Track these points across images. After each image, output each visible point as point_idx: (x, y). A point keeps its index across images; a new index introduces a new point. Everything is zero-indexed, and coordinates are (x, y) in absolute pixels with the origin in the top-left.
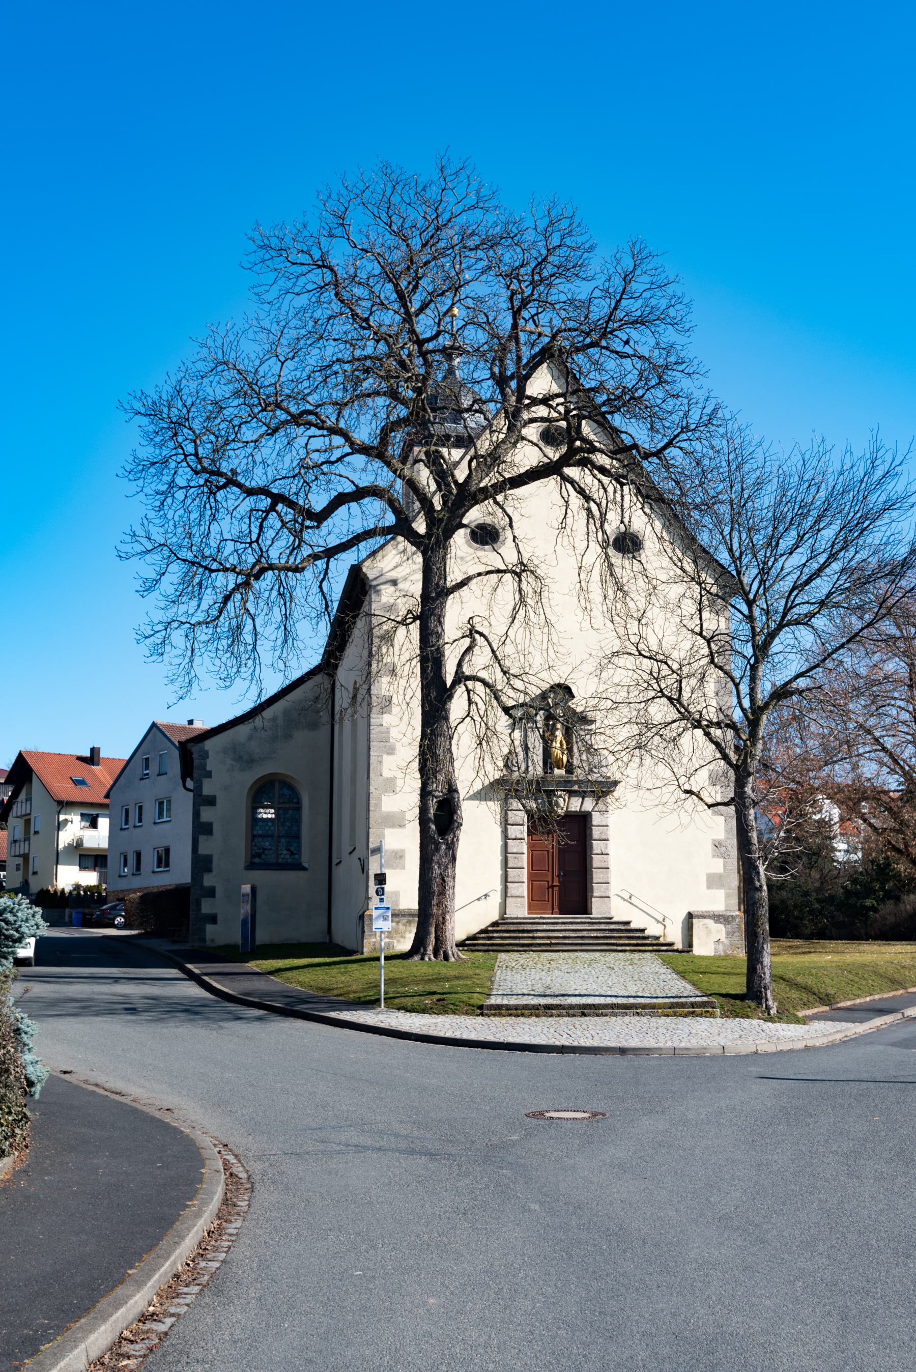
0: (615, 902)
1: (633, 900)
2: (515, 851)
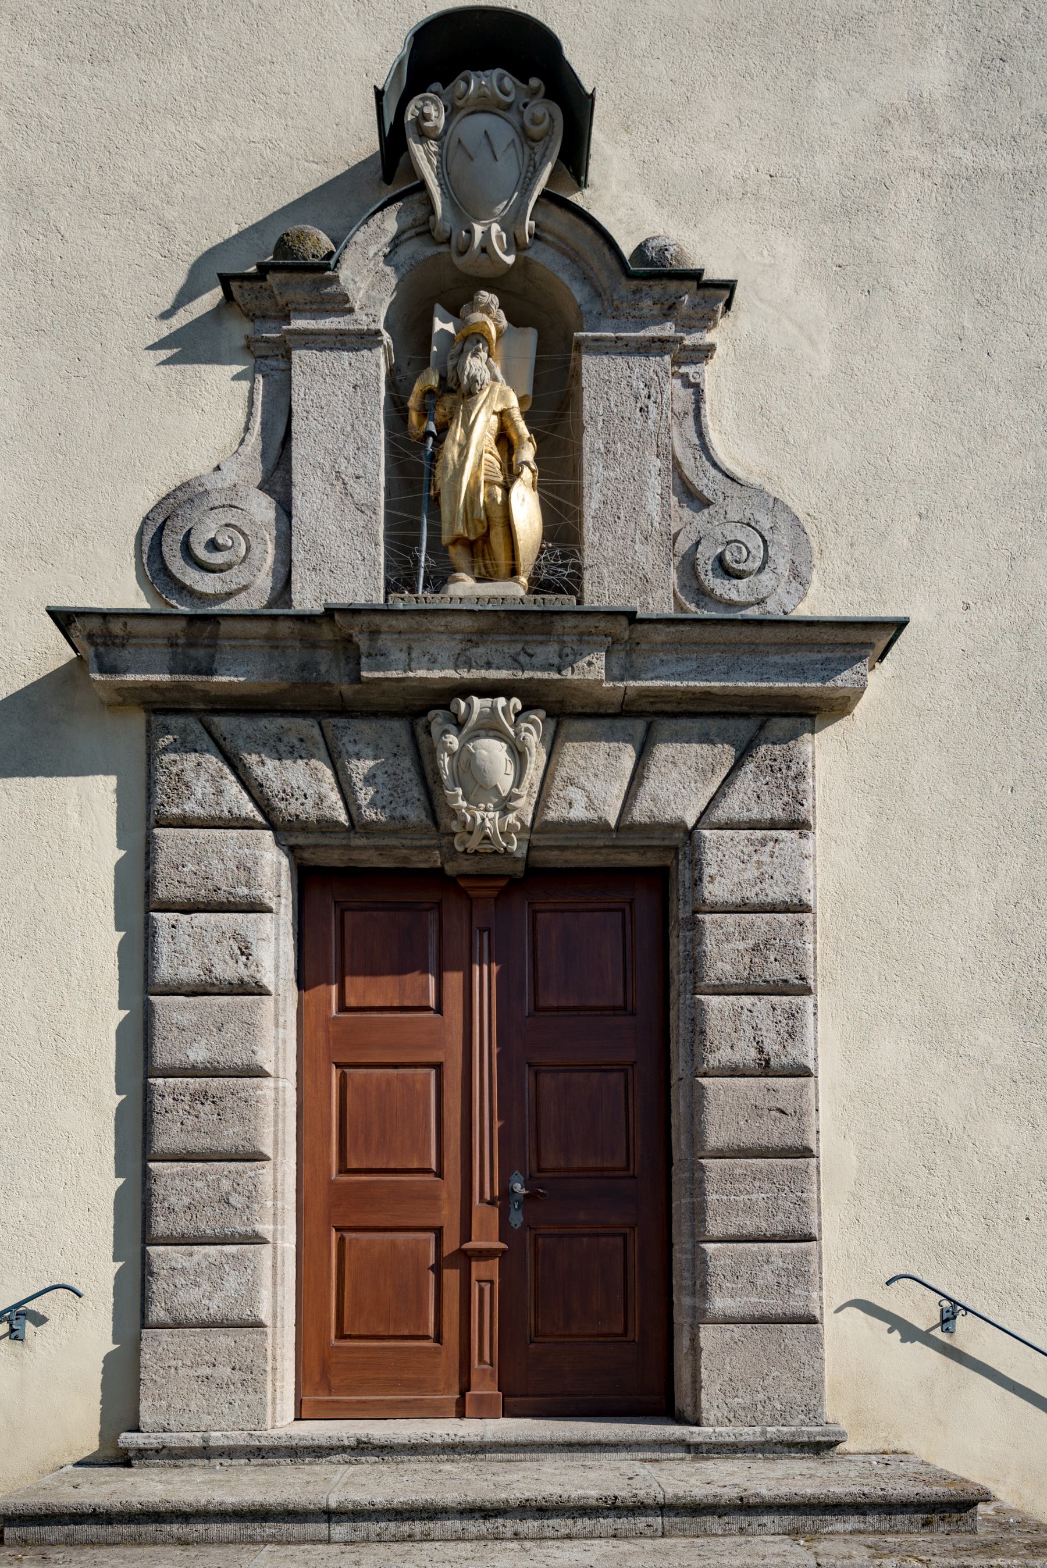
0: (848, 1343)
1: (967, 1334)
2: (198, 1054)
